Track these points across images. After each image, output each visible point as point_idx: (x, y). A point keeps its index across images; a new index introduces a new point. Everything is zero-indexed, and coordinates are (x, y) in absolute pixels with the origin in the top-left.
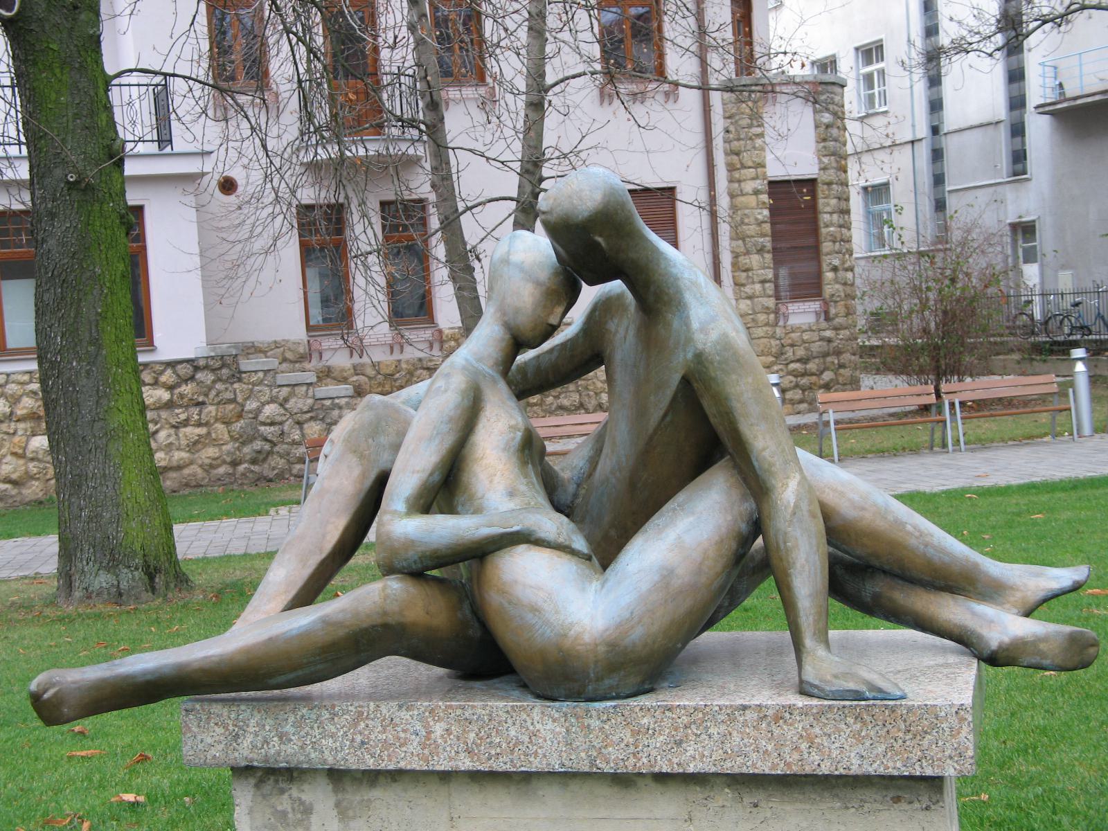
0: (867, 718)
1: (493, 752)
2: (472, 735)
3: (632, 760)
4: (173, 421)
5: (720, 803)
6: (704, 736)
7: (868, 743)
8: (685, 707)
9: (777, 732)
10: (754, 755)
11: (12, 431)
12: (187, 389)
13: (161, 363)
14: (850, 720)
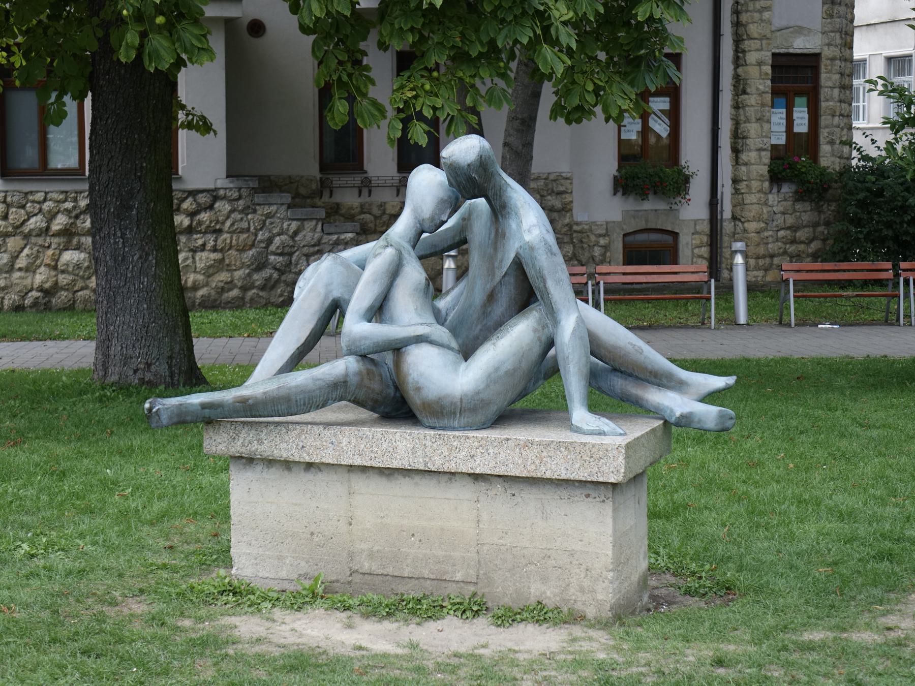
0: (572, 449)
1: (373, 456)
2: (362, 446)
3: (447, 465)
4: (191, 245)
5: (494, 493)
6: (485, 454)
7: (571, 463)
8: (476, 437)
9: (524, 453)
10: (511, 466)
11: (47, 245)
12: (204, 216)
13: (184, 191)
14: (563, 449)
